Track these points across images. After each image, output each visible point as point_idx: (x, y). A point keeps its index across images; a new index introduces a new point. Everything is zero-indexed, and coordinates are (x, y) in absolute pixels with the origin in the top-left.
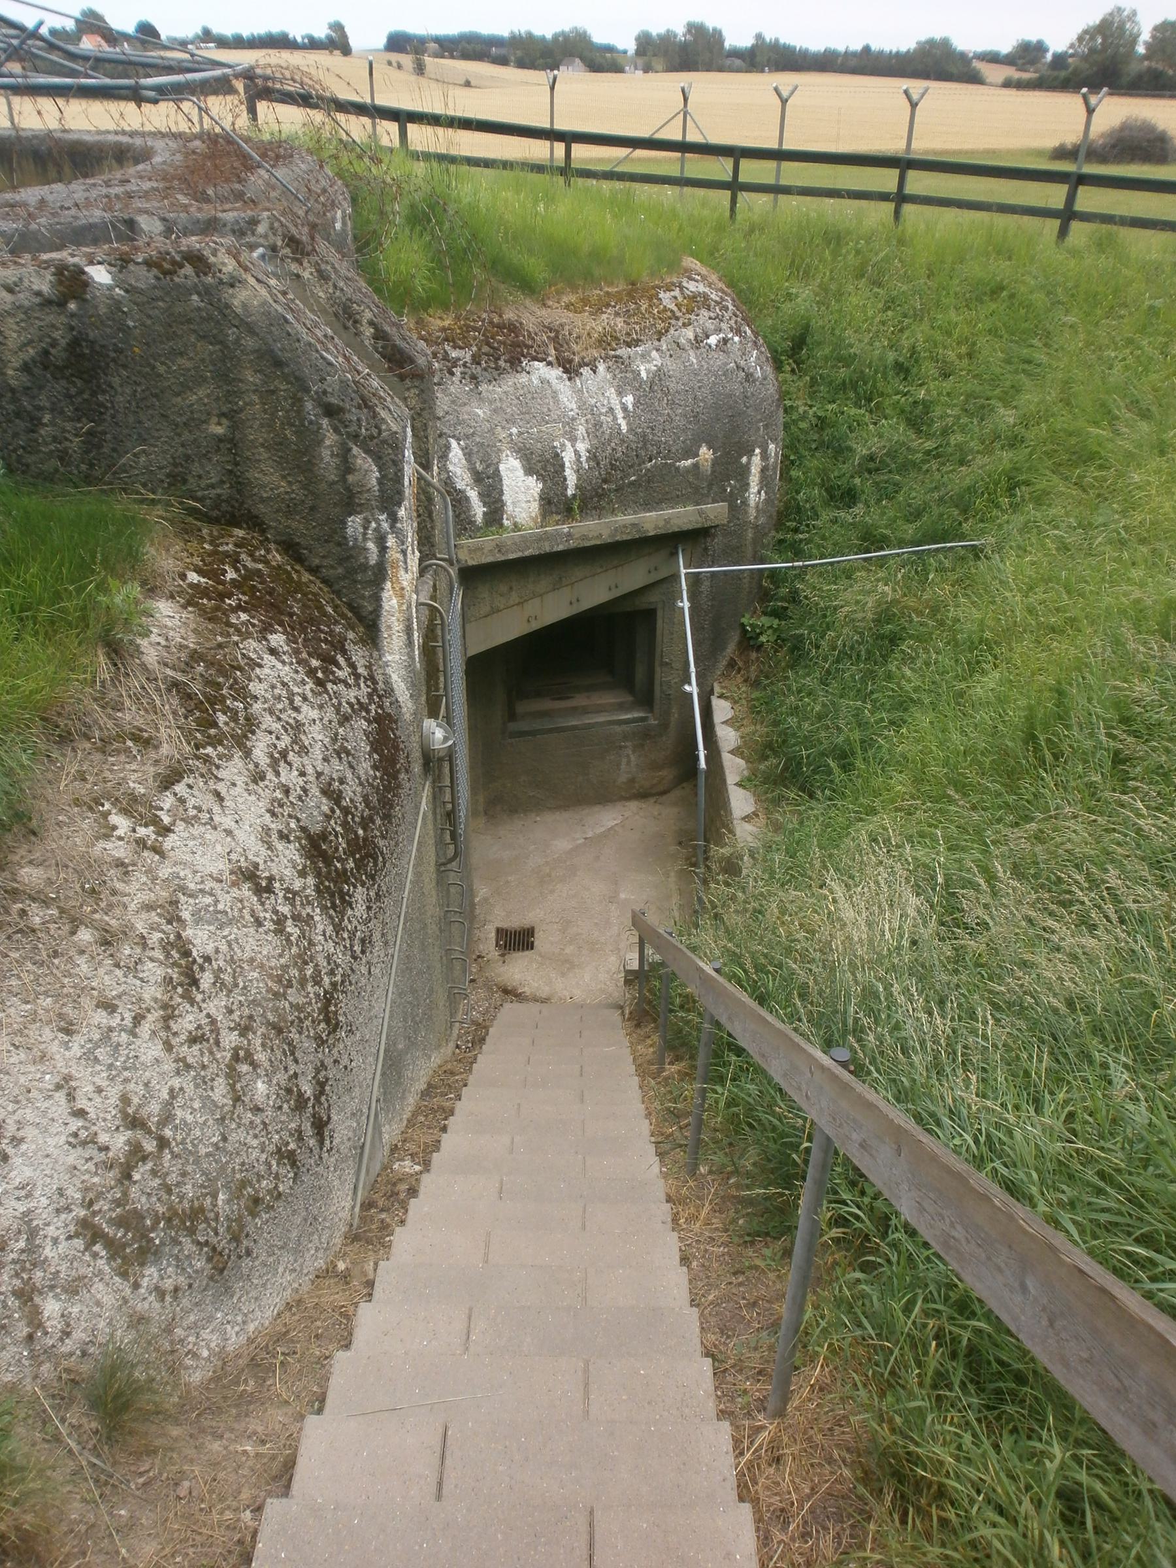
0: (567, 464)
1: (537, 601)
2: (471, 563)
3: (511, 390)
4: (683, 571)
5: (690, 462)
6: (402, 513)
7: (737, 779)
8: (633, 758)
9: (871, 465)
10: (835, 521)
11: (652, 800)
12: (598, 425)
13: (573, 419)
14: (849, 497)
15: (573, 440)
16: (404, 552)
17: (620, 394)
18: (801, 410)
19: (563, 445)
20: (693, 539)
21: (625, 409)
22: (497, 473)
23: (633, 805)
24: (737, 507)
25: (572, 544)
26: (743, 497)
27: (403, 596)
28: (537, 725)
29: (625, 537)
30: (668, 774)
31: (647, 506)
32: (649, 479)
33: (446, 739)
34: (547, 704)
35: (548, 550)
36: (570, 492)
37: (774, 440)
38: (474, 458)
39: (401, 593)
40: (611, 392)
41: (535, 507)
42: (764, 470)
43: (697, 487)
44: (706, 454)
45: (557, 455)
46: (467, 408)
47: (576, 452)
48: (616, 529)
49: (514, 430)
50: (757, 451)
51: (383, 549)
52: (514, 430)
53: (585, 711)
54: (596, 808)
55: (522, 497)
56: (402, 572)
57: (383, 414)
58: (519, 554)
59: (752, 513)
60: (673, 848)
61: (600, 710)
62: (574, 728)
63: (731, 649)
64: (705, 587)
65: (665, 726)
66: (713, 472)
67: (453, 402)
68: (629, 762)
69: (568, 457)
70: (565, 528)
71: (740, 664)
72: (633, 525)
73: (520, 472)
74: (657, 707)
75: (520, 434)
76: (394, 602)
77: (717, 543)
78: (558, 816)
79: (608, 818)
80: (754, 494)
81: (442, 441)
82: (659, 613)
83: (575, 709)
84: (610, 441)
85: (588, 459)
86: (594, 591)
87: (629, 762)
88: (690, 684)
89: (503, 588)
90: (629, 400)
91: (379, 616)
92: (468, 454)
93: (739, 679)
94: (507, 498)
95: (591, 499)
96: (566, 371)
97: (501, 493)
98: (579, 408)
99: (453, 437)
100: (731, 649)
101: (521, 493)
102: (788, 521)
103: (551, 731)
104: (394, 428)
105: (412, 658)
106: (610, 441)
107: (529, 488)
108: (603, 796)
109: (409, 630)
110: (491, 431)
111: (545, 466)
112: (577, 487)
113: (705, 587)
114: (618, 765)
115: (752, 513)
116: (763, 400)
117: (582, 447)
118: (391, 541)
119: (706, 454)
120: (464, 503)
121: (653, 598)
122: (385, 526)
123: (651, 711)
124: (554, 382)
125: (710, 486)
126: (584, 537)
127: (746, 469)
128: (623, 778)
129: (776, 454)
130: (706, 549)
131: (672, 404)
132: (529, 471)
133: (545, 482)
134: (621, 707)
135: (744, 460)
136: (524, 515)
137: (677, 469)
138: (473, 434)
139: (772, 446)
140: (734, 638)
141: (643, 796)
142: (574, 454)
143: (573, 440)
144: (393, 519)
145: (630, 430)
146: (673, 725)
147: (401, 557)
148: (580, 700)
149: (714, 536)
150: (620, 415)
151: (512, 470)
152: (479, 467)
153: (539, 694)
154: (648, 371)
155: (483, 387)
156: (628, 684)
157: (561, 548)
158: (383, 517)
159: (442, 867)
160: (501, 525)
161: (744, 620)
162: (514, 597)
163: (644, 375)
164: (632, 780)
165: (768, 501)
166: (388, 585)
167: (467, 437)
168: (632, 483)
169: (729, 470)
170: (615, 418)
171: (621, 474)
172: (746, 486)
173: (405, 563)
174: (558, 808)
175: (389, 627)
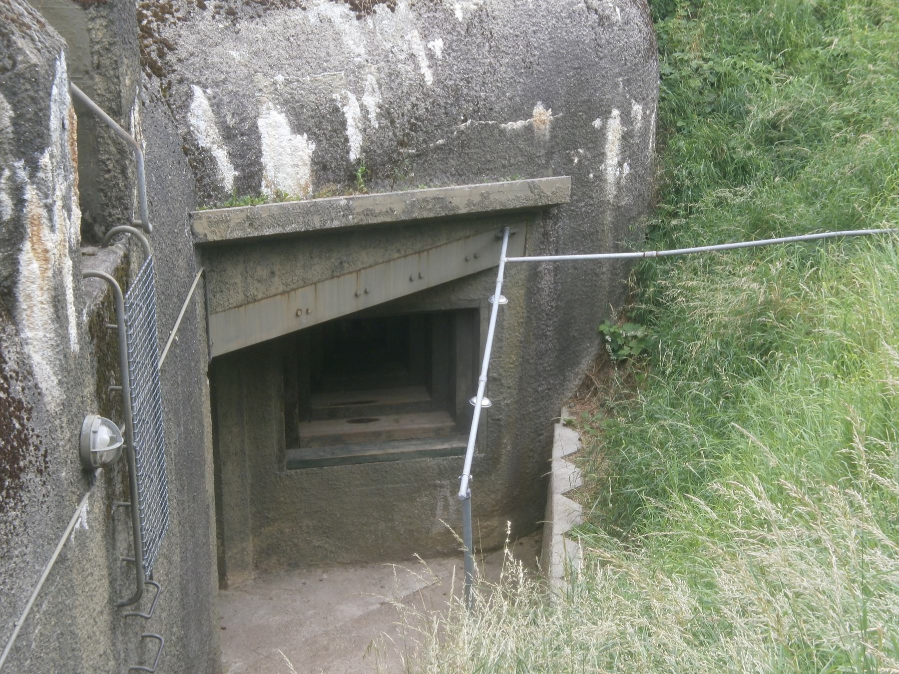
0: (350, 122)
1: (309, 290)
2: (211, 237)
3: (280, 29)
4: (504, 259)
5: (519, 124)
6: (45, 160)
7: (567, 527)
9: (772, 134)
10: (720, 203)
12: (394, 75)
13: (360, 67)
14: (742, 173)
15: (359, 92)
16: (49, 208)
17: (425, 36)
18: (694, 64)
19: (345, 98)
20: (527, 218)
21: (431, 56)
22: (254, 129)
24: (586, 180)
25: (352, 220)
26: (597, 170)
27: (47, 260)
28: (326, 453)
29: (426, 214)
31: (460, 176)
32: (464, 143)
33: (113, 440)
34: (343, 427)
35: (318, 225)
36: (353, 156)
37: (642, 100)
38: (225, 110)
39: (44, 256)
40: (414, 36)
41: (305, 173)
42: (626, 137)
43: (530, 156)
44: (542, 115)
45: (336, 110)
46: (219, 49)
47: (363, 108)
48: (413, 204)
49: (280, 78)
50: (616, 112)
51: (19, 202)
52: (280, 78)
53: (390, 437)
55: (287, 160)
56: (45, 231)
57: (21, 43)
58: (279, 230)
59: (611, 191)
61: (410, 437)
62: (374, 458)
63: (586, 363)
64: (547, 282)
66: (553, 137)
67: (202, 41)
69: (351, 112)
70: (342, 200)
72: (437, 199)
73: (286, 129)
75: (288, 82)
76: (35, 266)
77: (563, 226)
78: (352, 574)
80: (613, 167)
81: (184, 88)
83: (378, 434)
84: (409, 94)
85: (379, 116)
86: (388, 281)
88: (174, 340)
89: (262, 272)
90: (437, 45)
91: (15, 283)
92: (216, 105)
93: (594, 403)
94: (268, 159)
95: (378, 168)
96: (355, 8)
97: (259, 154)
98: (369, 53)
99: (198, 83)
100: (586, 363)
101: (287, 157)
102: (663, 205)
103: (343, 461)
104: (34, 59)
105: (64, 337)
106: (409, 94)
107: (296, 149)
109: (58, 302)
110: (249, 77)
111: (319, 123)
112: (364, 150)
113: (547, 282)
114: (433, 509)
115: (611, 191)
116: (623, 49)
117: (371, 101)
118: (30, 193)
119: (542, 115)
120: (208, 164)
122: (23, 175)
124: (337, 21)
125: (550, 154)
126: (369, 212)
127: (598, 138)
129: (646, 118)
130: (545, 234)
131: (496, 51)
132: (298, 128)
133: (319, 142)
135: (597, 123)
136: (289, 182)
137: (502, 132)
138: (224, 81)
139: (637, 109)
142: (360, 113)
143: (359, 92)
144: (34, 167)
145: (438, 82)
146: (504, 459)
147: (44, 213)
148: (385, 424)
149: (557, 218)
150: (424, 63)
151: (276, 126)
152: (230, 121)
153: (332, 415)
154: (465, 11)
155: (242, 25)
157: (336, 224)
158: (20, 164)
159: (116, 607)
160: (259, 194)
161: (604, 328)
162: (278, 285)
163: (459, 15)
165: (633, 177)
166: (27, 246)
167: (216, 84)
168: (439, 148)
169: (576, 134)
170: (417, 67)
171: (416, 138)
172: (601, 156)
173: (51, 220)
174: (353, 563)
175: (29, 297)
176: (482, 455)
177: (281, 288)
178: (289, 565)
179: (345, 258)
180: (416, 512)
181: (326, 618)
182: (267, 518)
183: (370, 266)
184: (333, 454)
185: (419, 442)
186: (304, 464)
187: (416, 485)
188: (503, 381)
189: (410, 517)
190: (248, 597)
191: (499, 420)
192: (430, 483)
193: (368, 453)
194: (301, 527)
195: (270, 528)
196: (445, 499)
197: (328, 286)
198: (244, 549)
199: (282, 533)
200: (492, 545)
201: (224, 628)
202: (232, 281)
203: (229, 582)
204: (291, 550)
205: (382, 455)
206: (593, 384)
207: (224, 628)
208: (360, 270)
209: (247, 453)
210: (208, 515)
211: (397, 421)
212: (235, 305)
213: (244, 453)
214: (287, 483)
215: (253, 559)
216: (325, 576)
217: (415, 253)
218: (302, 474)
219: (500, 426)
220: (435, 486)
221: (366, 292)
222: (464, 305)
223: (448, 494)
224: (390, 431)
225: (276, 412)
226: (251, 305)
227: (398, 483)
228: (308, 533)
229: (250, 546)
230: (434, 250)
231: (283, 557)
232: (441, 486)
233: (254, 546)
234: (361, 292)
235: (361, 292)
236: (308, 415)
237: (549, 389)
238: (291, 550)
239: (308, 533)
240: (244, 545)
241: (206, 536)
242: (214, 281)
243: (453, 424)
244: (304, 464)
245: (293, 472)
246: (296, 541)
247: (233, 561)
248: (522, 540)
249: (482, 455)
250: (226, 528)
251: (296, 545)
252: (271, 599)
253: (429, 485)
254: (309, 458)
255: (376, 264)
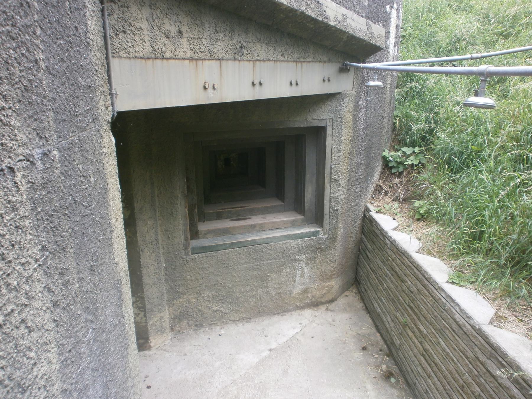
1: (214, 64)
8: (306, 270)
11: (323, 308)
23: (308, 313)
30: (335, 284)
34: (228, 224)
53: (262, 228)
54: (276, 318)
60: (358, 355)
61: (275, 227)
62: (254, 243)
65: (333, 239)
68: (302, 275)
71: (386, 188)
74: (326, 222)
79: (288, 327)
82: (329, 131)
83: (253, 227)
87: (302, 275)
103: (232, 245)
108: (281, 307)
121: (321, 116)
123: (322, 226)
128: (298, 289)
134: (294, 224)
140: (379, 167)
141: (315, 304)
148: (256, 220)
153: (219, 216)
156: (298, 206)
164: (306, 291)
174: (241, 320)
176: (326, 236)
177: (189, 54)
178: (196, 326)
179: (244, 44)
180: (283, 279)
181: (231, 368)
182: (178, 292)
183: (264, 61)
184: (224, 241)
185: (283, 230)
186: (204, 249)
187: (283, 260)
188: (340, 182)
189: (279, 284)
190: (167, 355)
191: (337, 210)
192: (292, 258)
193: (250, 239)
194: (203, 297)
195: (181, 300)
196: (302, 268)
197: (230, 67)
198: (162, 317)
199: (190, 302)
200: (330, 298)
201: (149, 387)
202: (137, 25)
203: (152, 344)
204: (197, 315)
205: (259, 239)
206: (382, 189)
207: (149, 387)
208: (256, 61)
209: (160, 242)
210: (120, 291)
211: (264, 218)
212: (141, 55)
213: (158, 242)
214: (192, 264)
215: (170, 324)
216: (223, 332)
217: (294, 61)
218: (202, 257)
219: (337, 215)
220: (296, 260)
221: (261, 84)
222: (315, 124)
223: (304, 265)
224: (262, 224)
225: (181, 209)
226: (158, 62)
227: (270, 260)
228: (209, 301)
229: (166, 315)
230: (305, 63)
231: (189, 320)
232: (300, 260)
233: (170, 315)
234: (257, 82)
235: (257, 82)
236: (204, 217)
237: (361, 191)
238: (197, 315)
239: (209, 301)
240: (162, 314)
241: (119, 315)
242: (115, 16)
243: (303, 217)
244: (204, 249)
245: (196, 256)
246: (200, 308)
247: (154, 328)
248: (347, 293)
249: (326, 236)
250: (147, 303)
251: (200, 311)
252: (185, 355)
253: (292, 260)
254: (207, 245)
255: (268, 60)
